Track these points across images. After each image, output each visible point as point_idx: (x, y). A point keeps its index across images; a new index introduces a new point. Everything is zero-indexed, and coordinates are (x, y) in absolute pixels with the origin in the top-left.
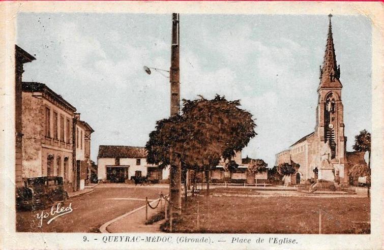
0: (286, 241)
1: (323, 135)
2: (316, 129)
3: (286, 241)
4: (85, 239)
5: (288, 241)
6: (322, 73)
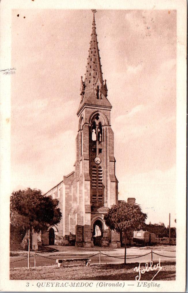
0: (153, 285)
1: (88, 172)
2: (76, 165)
3: (153, 285)
4: (8, 120)
5: (155, 285)
6: (84, 86)
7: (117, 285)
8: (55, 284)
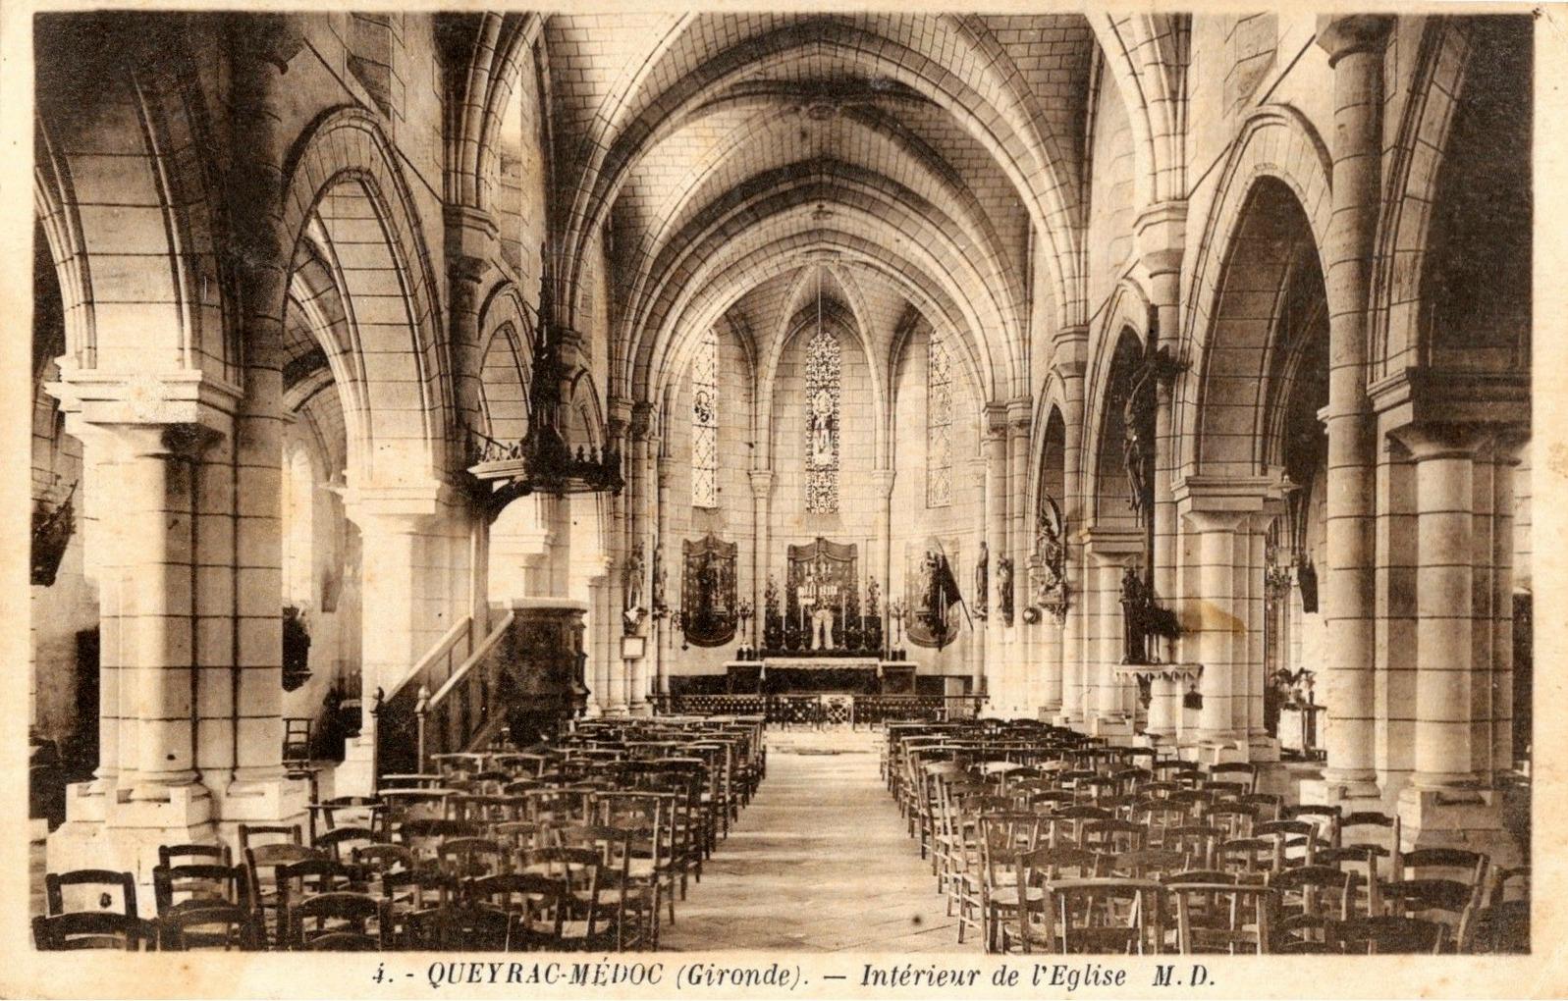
5: (1102, 977)
7: (768, 979)
8: (506, 969)
